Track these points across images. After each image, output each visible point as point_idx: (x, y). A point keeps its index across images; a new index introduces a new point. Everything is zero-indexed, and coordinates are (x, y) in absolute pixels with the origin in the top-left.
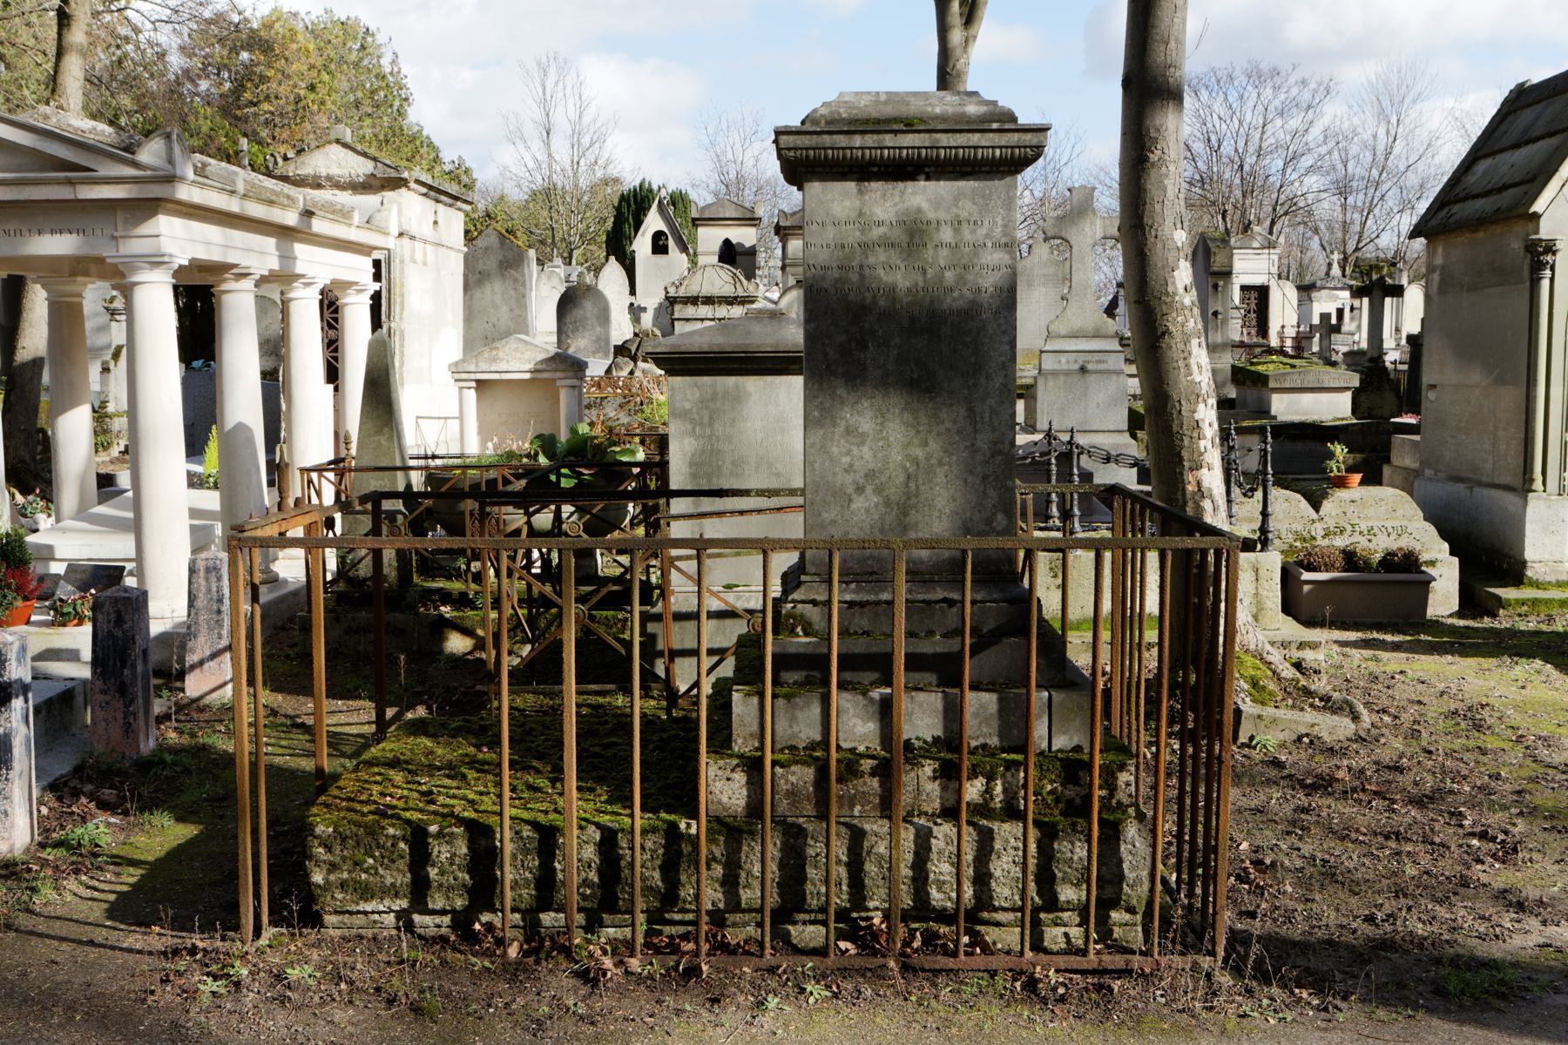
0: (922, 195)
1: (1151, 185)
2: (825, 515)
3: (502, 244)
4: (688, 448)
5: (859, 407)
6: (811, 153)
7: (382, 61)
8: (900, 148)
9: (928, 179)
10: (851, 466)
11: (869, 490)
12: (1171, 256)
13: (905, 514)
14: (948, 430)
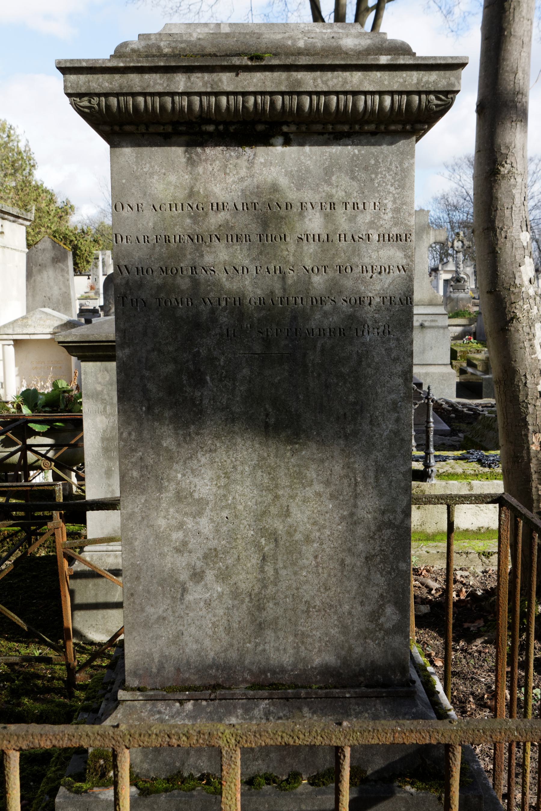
0: (276, 165)
1: (501, 194)
2: (150, 610)
3: (54, 247)
4: (100, 426)
5: (194, 464)
6: (114, 101)
7: (20, 145)
8: (244, 94)
9: (287, 143)
10: (185, 544)
11: (210, 576)
12: (518, 254)
13: (261, 608)
14: (319, 494)
